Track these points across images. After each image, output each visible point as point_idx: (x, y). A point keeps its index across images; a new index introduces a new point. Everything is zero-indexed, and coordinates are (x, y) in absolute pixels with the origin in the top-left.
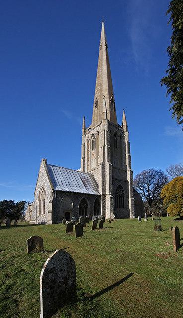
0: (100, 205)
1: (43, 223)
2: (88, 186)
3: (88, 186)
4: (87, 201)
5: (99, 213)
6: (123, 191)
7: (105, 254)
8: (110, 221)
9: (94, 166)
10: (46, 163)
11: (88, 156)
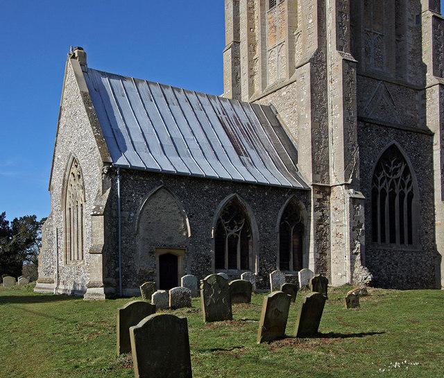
0: (302, 231)
1: (77, 295)
2: (253, 153)
3: (253, 153)
4: (249, 212)
5: (300, 264)
6: (407, 171)
7: (400, 300)
8: (353, 301)
9: (277, 71)
10: (83, 65)
11: (251, 36)
